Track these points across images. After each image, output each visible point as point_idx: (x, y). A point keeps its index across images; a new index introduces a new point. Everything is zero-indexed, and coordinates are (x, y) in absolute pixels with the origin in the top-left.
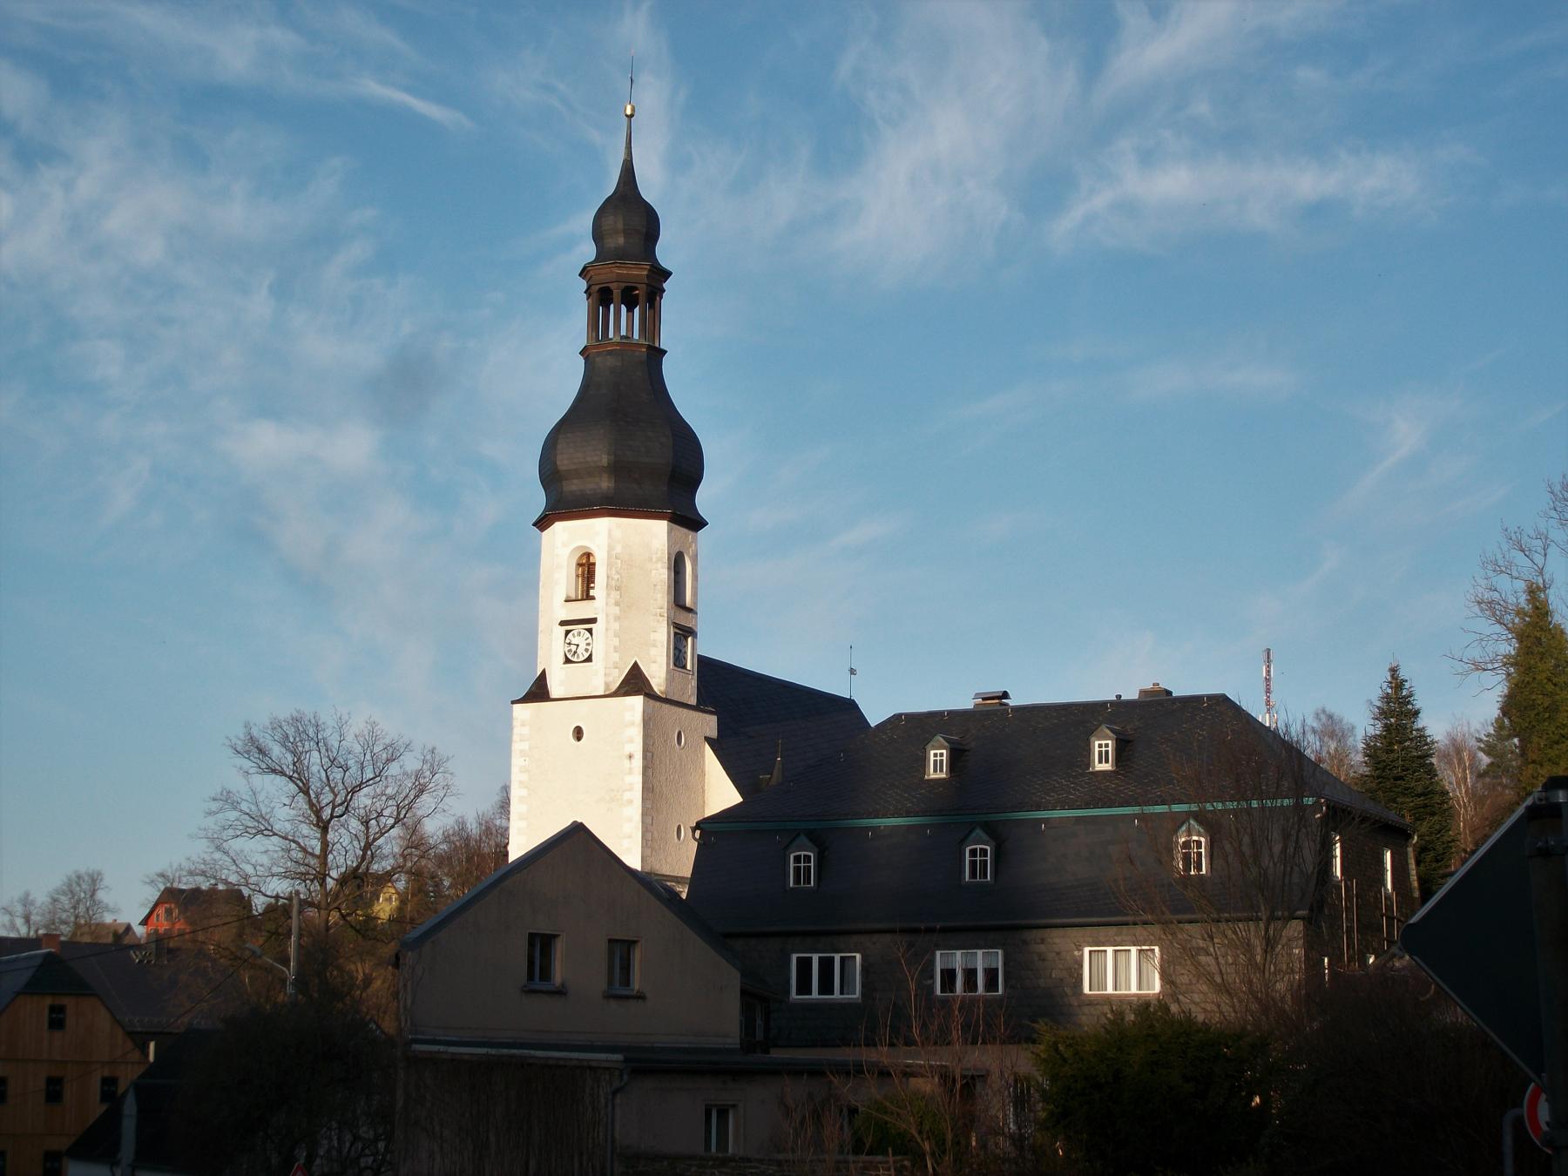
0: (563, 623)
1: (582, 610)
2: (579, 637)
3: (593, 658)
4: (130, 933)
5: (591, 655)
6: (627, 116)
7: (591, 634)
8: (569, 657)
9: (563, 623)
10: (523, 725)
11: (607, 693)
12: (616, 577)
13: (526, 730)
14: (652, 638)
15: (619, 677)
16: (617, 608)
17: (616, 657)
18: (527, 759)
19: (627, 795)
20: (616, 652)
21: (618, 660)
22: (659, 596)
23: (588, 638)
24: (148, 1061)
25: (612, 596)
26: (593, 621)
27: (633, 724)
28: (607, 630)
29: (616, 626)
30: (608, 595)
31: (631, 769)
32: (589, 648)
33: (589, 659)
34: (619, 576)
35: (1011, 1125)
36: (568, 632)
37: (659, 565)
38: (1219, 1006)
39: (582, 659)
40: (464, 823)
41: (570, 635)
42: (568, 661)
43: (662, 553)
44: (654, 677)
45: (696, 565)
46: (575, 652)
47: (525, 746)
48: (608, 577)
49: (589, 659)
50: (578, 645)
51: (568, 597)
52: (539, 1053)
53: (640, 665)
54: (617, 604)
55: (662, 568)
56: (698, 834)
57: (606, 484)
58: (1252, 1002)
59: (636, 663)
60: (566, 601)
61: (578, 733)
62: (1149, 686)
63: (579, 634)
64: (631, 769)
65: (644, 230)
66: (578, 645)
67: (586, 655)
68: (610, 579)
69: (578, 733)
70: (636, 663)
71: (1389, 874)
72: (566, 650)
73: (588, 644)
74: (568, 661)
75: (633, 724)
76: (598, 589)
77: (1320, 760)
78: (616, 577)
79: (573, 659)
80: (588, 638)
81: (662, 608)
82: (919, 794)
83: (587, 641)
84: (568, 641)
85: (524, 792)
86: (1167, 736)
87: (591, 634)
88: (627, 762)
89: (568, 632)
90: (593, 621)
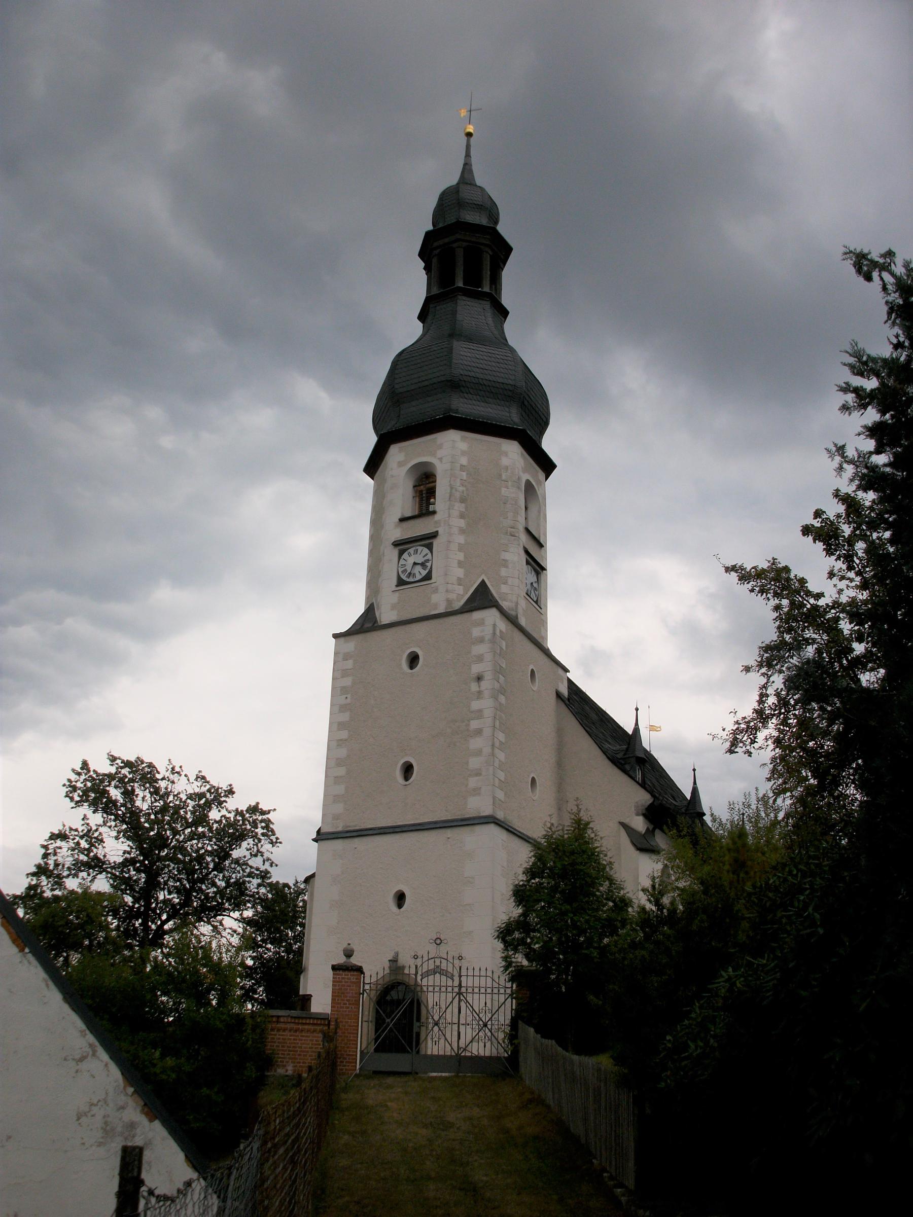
5: (430, 572)
7: (432, 552)
8: (404, 577)
16: (462, 521)
18: (349, 696)
19: (474, 725)
20: (460, 567)
21: (462, 576)
23: (427, 554)
24: (732, 967)
25: (456, 508)
34: (464, 489)
35: (899, 474)
36: (401, 553)
39: (418, 577)
44: (505, 600)
45: (465, 164)
49: (428, 577)
52: (415, 1008)
54: (462, 516)
56: (432, 500)
58: (792, 796)
59: (483, 581)
64: (480, 692)
68: (454, 491)
70: (483, 581)
72: (400, 570)
74: (401, 582)
76: (440, 503)
78: (461, 489)
80: (427, 554)
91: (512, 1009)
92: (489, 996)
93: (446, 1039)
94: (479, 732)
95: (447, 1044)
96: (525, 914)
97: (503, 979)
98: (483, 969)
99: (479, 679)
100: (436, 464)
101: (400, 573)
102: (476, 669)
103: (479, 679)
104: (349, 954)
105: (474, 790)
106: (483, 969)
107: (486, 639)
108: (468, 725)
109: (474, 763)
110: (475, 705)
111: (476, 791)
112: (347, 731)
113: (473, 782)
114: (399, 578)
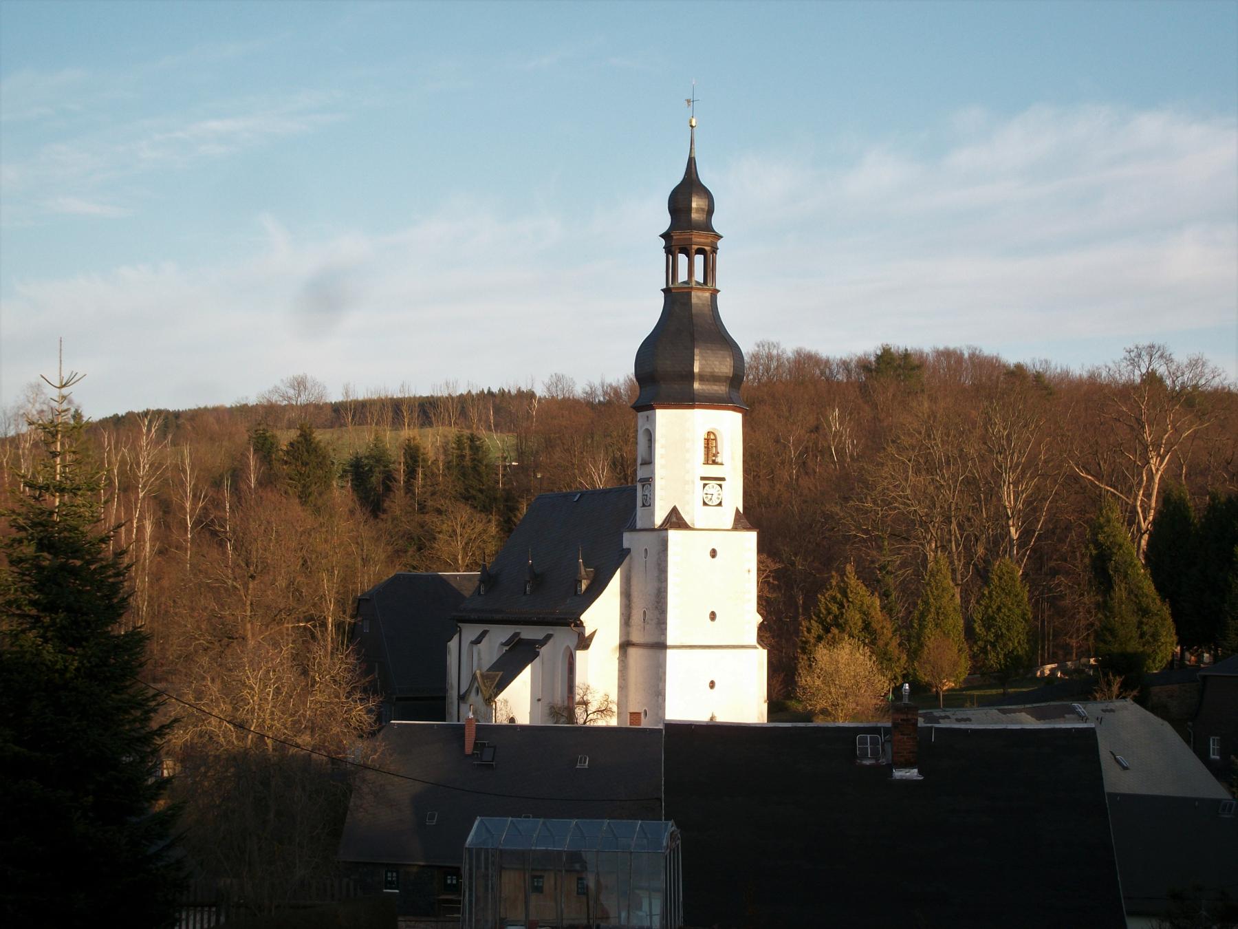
0: (703, 478)
1: (713, 471)
2: (713, 486)
3: (723, 504)
4: (663, 651)
7: (721, 487)
26: (723, 479)
32: (720, 497)
33: (720, 504)
36: (705, 485)
40: (349, 384)
41: (707, 487)
42: (705, 504)
46: (711, 499)
49: (720, 504)
61: (714, 553)
62: (104, 417)
63: (713, 487)
65: (707, 208)
67: (718, 502)
69: (714, 553)
73: (719, 494)
74: (705, 504)
77: (635, 716)
82: (845, 439)
83: (711, 487)
84: (705, 491)
87: (721, 487)
89: (705, 485)
90: (723, 479)
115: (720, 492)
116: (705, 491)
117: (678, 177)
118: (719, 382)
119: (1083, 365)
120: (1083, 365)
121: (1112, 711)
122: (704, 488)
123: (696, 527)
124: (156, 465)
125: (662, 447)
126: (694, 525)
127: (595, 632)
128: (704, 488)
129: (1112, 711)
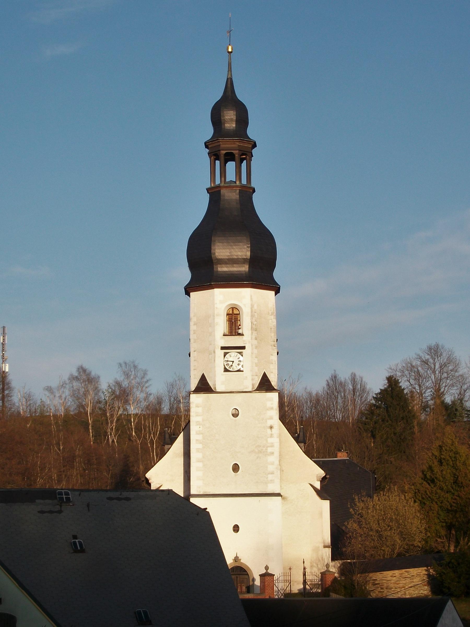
0: (223, 348)
2: (233, 355)
6: (229, 52)
8: (227, 368)
9: (223, 348)
10: (197, 406)
11: (253, 390)
12: (255, 323)
13: (200, 410)
14: (271, 359)
15: (258, 381)
17: (256, 369)
19: (270, 450)
22: (273, 334)
26: (243, 348)
27: (272, 408)
28: (252, 353)
29: (255, 351)
30: (252, 333)
31: (271, 434)
36: (225, 354)
37: (272, 317)
38: (317, 565)
41: (227, 356)
42: (226, 370)
43: (273, 310)
46: (232, 366)
47: (199, 419)
48: (252, 323)
50: (233, 362)
51: (224, 333)
53: (266, 373)
54: (256, 339)
55: (274, 318)
57: (245, 268)
60: (224, 335)
66: (233, 362)
68: (252, 324)
70: (265, 372)
71: (155, 454)
74: (226, 370)
75: (272, 408)
79: (230, 370)
81: (274, 342)
84: (226, 359)
85: (200, 446)
86: (420, 403)
88: (269, 430)
89: (225, 354)
90: (243, 348)
91: (240, 321)
92: (283, 583)
93: (276, 586)
94: (272, 453)
95: (276, 588)
96: (325, 476)
97: (425, 578)
98: (287, 573)
99: (271, 427)
100: (243, 308)
101: (225, 365)
102: (270, 423)
103: (271, 427)
104: (267, 568)
105: (271, 481)
106: (287, 573)
107: (274, 408)
108: (266, 449)
109: (271, 468)
110: (270, 440)
111: (272, 481)
112: (201, 444)
113: (270, 477)
114: (225, 368)
115: (241, 358)
116: (226, 359)
117: (218, 95)
118: (238, 264)
119: (385, 369)
120: (385, 369)
121: (128, 499)
122: (225, 356)
123: (218, 390)
124: (94, 481)
125: (197, 434)
126: (215, 388)
127: (309, 484)
128: (225, 356)
129: (128, 499)
